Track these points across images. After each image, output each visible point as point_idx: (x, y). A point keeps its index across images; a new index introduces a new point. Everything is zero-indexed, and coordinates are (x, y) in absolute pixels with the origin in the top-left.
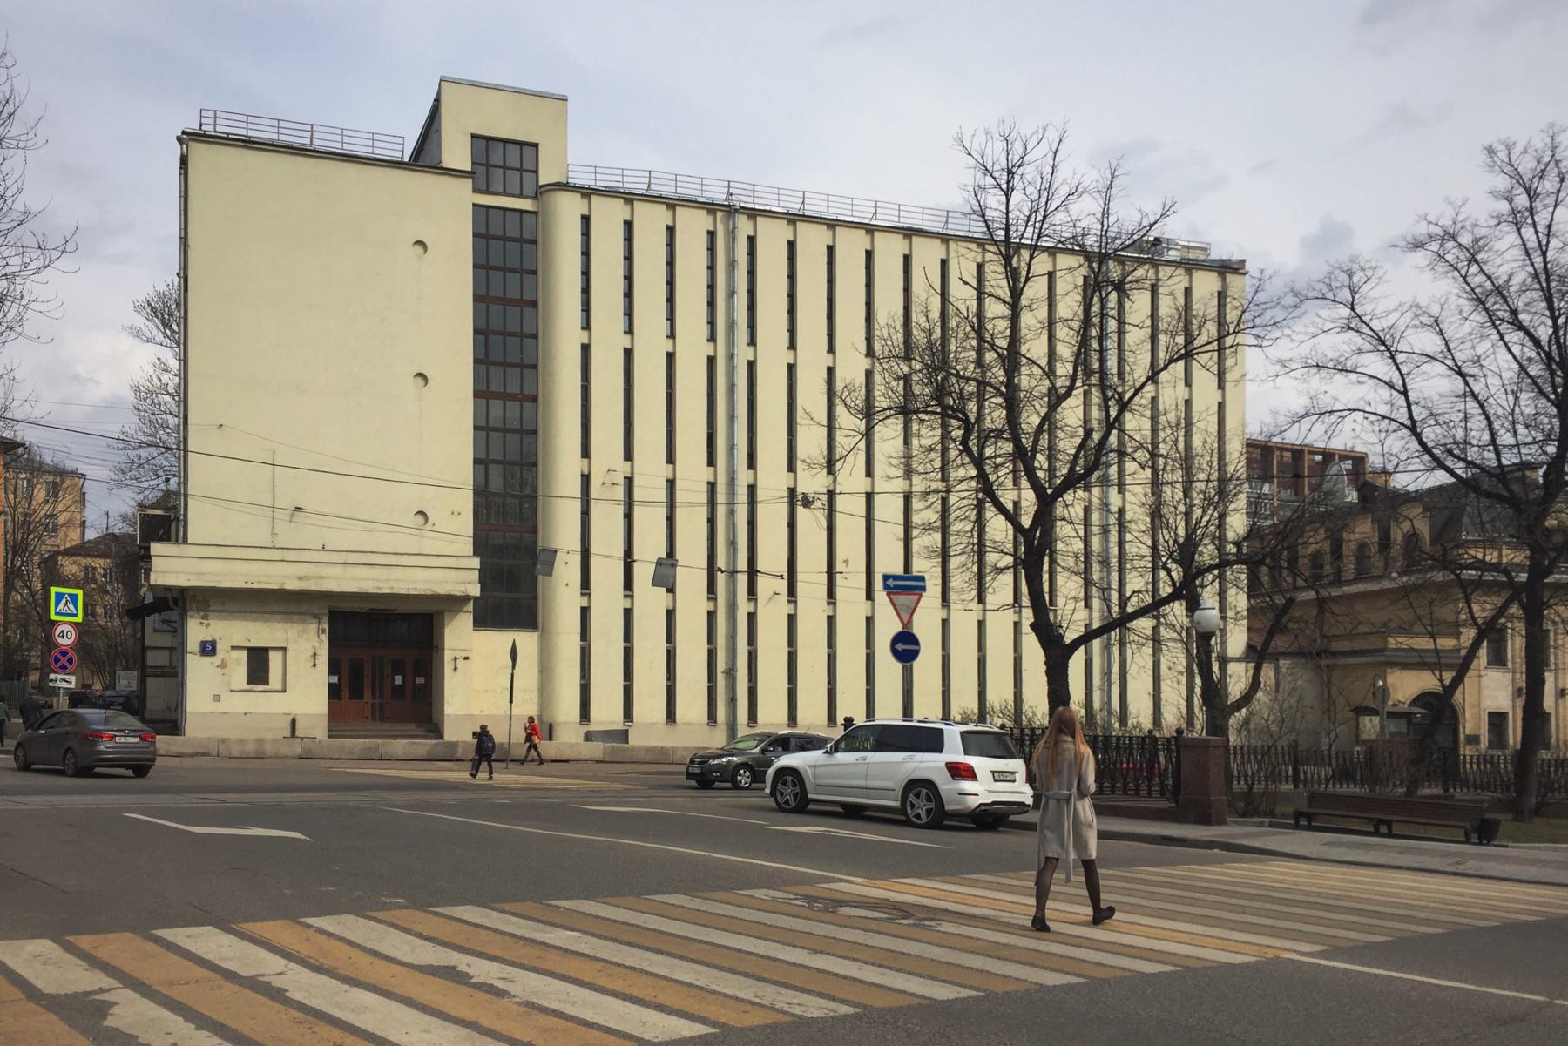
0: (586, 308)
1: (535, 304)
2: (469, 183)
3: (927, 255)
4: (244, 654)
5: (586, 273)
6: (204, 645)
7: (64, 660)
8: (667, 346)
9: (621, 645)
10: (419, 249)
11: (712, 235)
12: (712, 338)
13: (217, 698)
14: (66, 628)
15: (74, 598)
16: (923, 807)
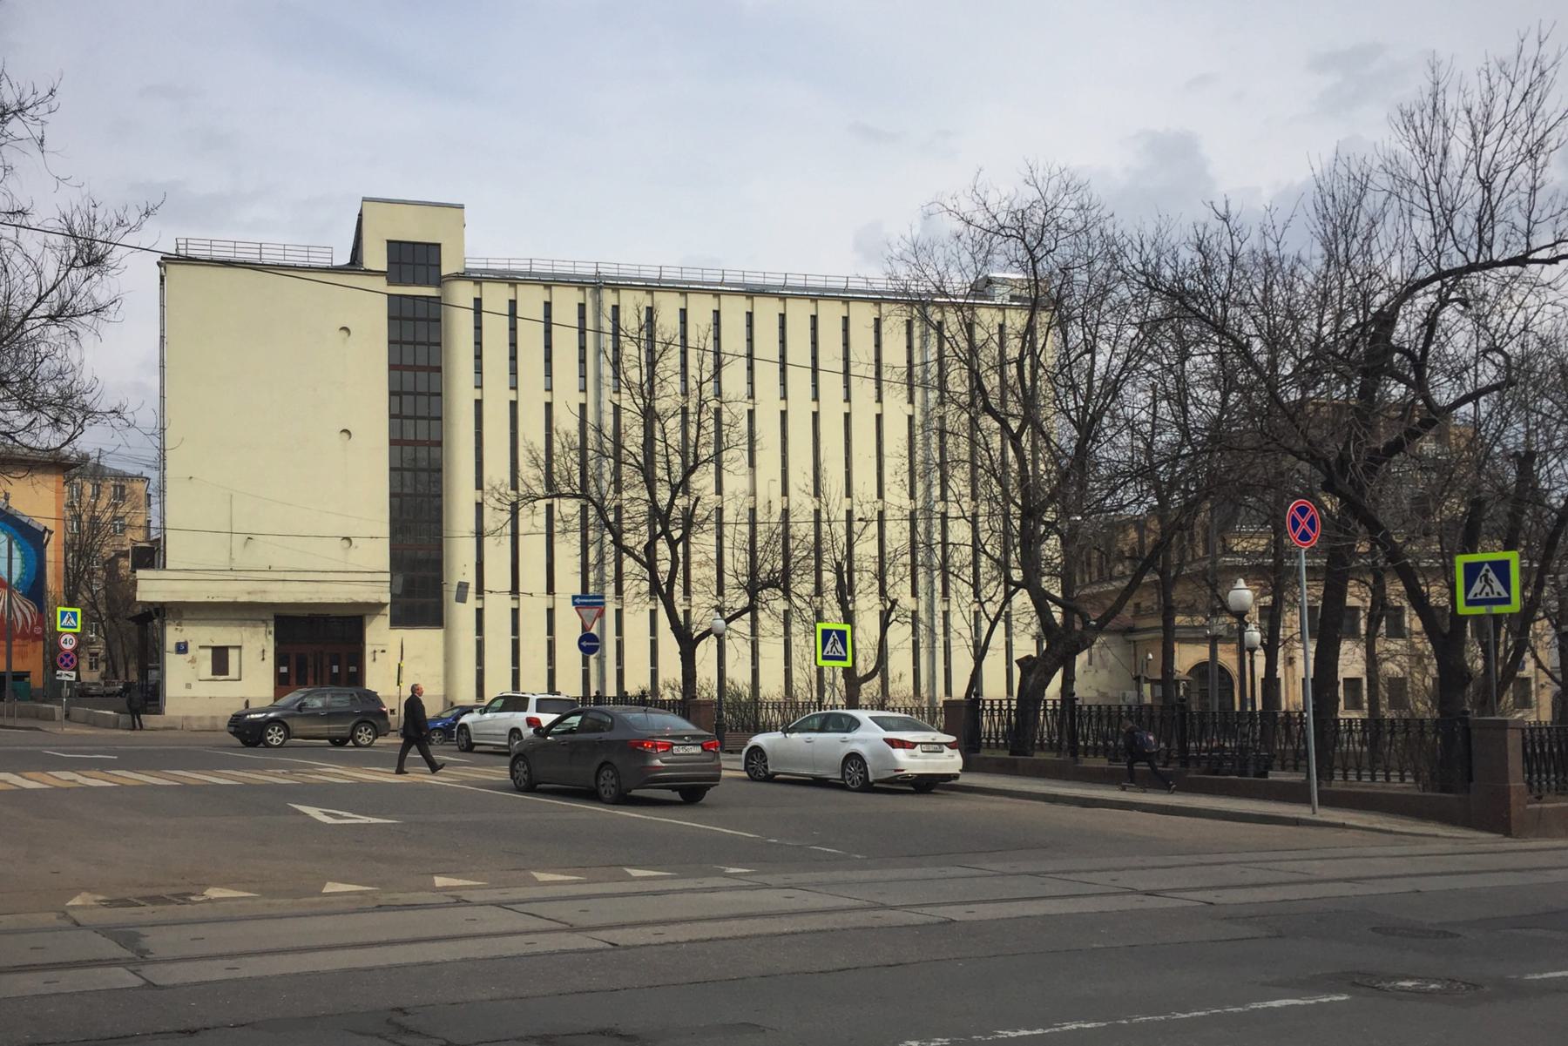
0: (479, 370)
1: (439, 369)
2: (383, 280)
3: (701, 310)
4: (209, 652)
5: (478, 343)
6: (178, 645)
7: (67, 661)
8: (845, 408)
9: (509, 638)
10: (344, 333)
11: (582, 307)
12: (584, 390)
13: (188, 686)
14: (69, 637)
15: (74, 614)
16: (854, 775)
